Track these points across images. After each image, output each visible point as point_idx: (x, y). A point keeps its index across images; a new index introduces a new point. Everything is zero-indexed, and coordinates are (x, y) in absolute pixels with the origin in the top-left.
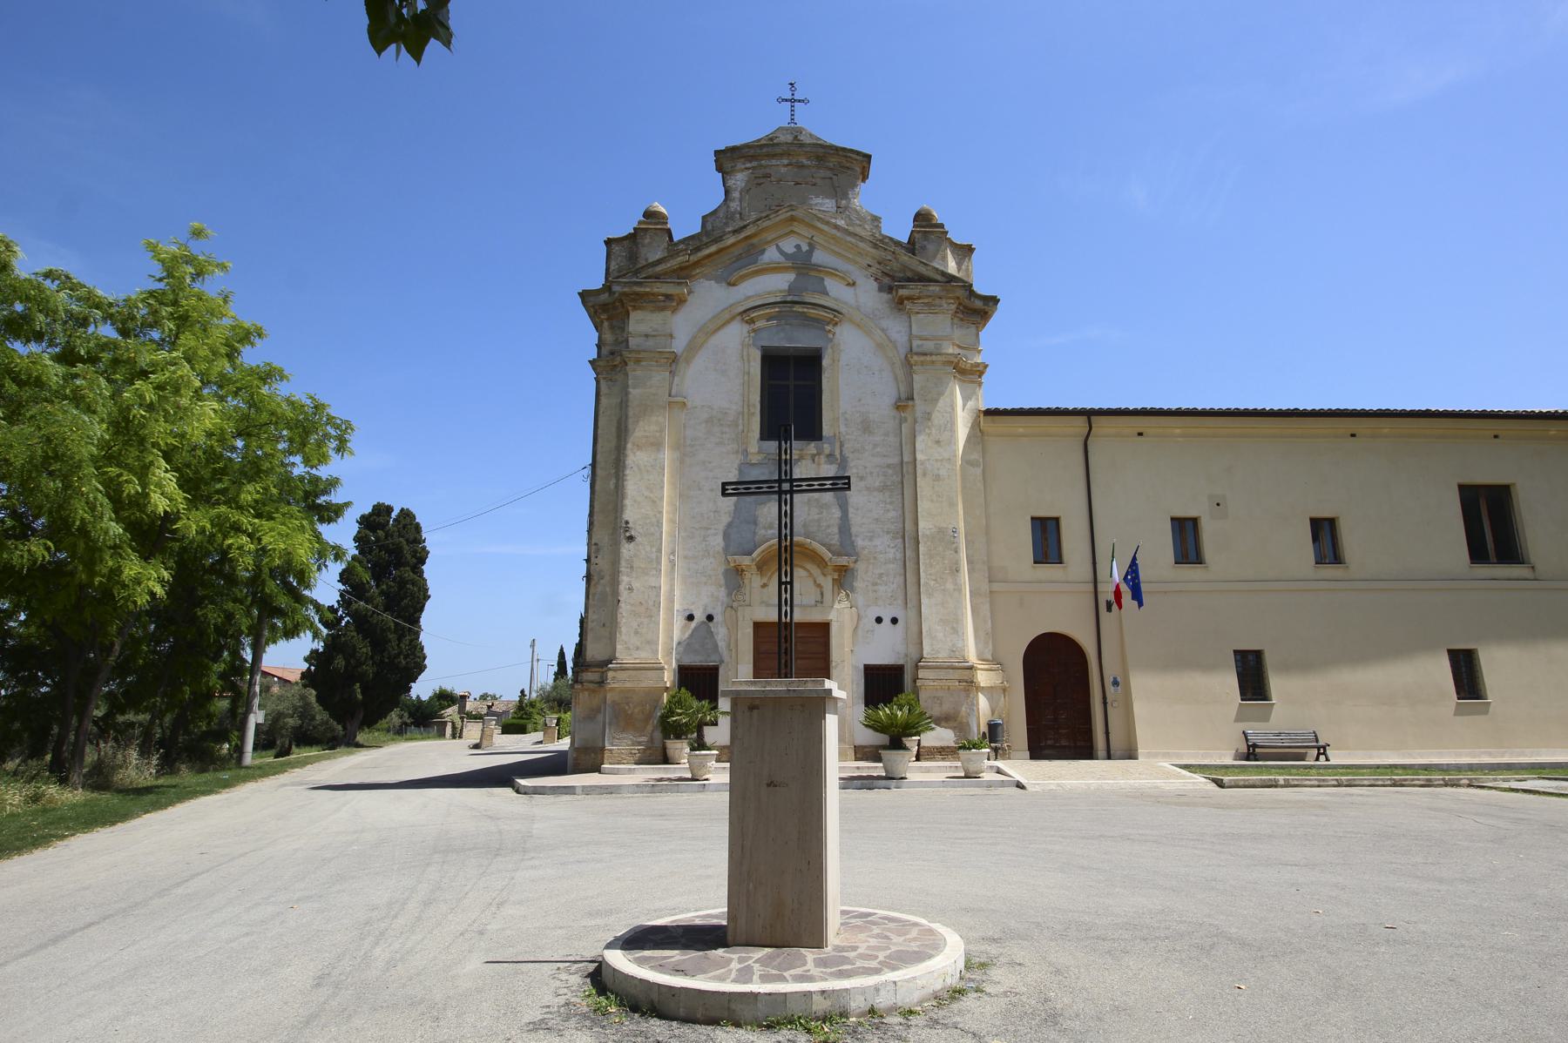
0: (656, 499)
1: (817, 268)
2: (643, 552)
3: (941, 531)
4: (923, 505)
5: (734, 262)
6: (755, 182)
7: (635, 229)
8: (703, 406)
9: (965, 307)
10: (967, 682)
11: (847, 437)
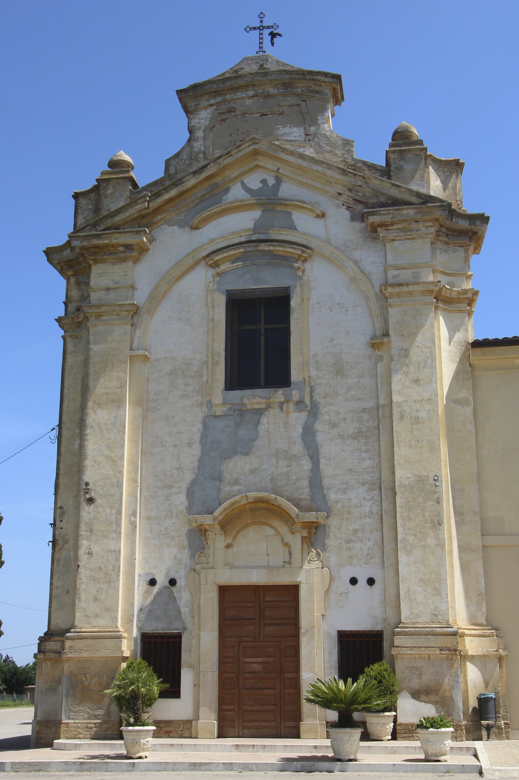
0: (116, 458)
1: (283, 202)
2: (103, 515)
3: (421, 480)
4: (400, 452)
5: (198, 204)
6: (220, 118)
7: (97, 180)
8: (166, 358)
9: (448, 229)
10: (449, 650)
11: (318, 381)
